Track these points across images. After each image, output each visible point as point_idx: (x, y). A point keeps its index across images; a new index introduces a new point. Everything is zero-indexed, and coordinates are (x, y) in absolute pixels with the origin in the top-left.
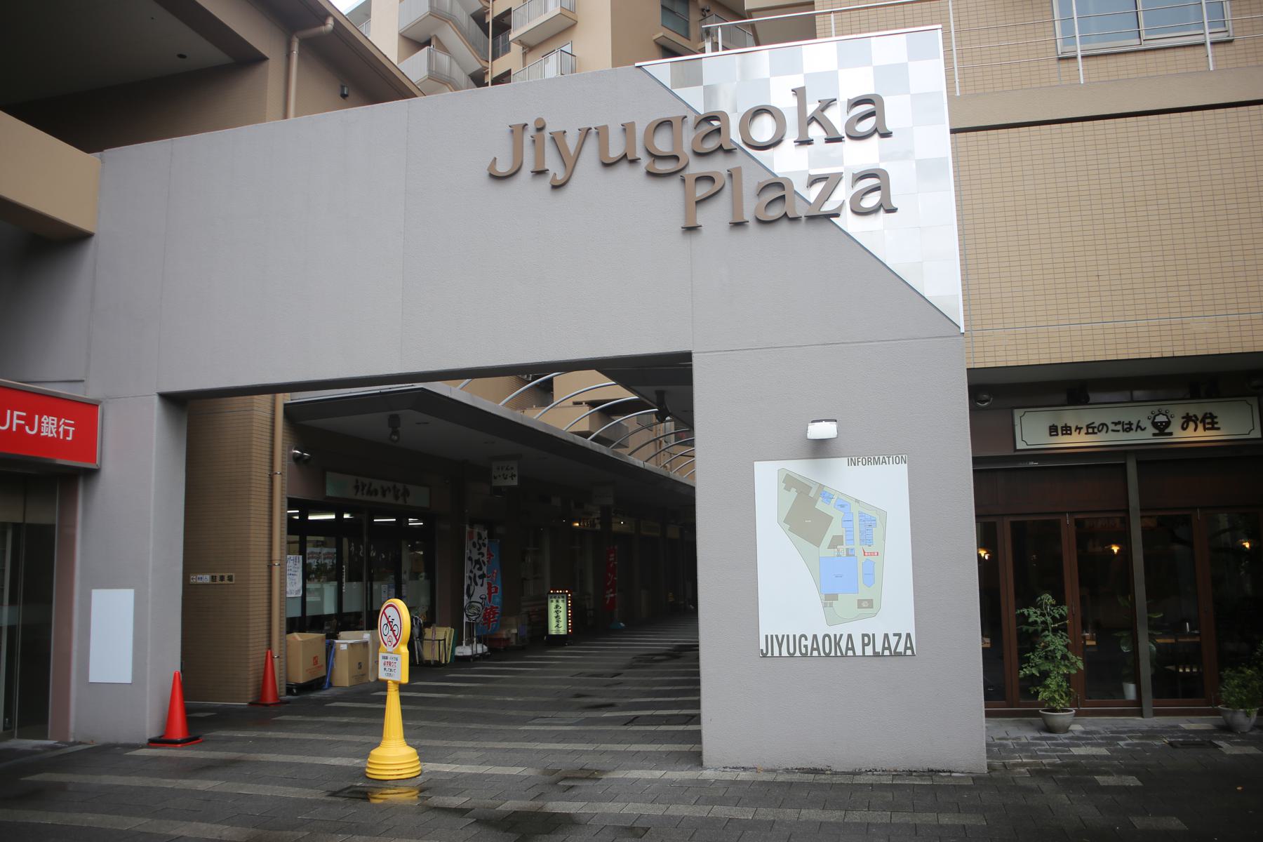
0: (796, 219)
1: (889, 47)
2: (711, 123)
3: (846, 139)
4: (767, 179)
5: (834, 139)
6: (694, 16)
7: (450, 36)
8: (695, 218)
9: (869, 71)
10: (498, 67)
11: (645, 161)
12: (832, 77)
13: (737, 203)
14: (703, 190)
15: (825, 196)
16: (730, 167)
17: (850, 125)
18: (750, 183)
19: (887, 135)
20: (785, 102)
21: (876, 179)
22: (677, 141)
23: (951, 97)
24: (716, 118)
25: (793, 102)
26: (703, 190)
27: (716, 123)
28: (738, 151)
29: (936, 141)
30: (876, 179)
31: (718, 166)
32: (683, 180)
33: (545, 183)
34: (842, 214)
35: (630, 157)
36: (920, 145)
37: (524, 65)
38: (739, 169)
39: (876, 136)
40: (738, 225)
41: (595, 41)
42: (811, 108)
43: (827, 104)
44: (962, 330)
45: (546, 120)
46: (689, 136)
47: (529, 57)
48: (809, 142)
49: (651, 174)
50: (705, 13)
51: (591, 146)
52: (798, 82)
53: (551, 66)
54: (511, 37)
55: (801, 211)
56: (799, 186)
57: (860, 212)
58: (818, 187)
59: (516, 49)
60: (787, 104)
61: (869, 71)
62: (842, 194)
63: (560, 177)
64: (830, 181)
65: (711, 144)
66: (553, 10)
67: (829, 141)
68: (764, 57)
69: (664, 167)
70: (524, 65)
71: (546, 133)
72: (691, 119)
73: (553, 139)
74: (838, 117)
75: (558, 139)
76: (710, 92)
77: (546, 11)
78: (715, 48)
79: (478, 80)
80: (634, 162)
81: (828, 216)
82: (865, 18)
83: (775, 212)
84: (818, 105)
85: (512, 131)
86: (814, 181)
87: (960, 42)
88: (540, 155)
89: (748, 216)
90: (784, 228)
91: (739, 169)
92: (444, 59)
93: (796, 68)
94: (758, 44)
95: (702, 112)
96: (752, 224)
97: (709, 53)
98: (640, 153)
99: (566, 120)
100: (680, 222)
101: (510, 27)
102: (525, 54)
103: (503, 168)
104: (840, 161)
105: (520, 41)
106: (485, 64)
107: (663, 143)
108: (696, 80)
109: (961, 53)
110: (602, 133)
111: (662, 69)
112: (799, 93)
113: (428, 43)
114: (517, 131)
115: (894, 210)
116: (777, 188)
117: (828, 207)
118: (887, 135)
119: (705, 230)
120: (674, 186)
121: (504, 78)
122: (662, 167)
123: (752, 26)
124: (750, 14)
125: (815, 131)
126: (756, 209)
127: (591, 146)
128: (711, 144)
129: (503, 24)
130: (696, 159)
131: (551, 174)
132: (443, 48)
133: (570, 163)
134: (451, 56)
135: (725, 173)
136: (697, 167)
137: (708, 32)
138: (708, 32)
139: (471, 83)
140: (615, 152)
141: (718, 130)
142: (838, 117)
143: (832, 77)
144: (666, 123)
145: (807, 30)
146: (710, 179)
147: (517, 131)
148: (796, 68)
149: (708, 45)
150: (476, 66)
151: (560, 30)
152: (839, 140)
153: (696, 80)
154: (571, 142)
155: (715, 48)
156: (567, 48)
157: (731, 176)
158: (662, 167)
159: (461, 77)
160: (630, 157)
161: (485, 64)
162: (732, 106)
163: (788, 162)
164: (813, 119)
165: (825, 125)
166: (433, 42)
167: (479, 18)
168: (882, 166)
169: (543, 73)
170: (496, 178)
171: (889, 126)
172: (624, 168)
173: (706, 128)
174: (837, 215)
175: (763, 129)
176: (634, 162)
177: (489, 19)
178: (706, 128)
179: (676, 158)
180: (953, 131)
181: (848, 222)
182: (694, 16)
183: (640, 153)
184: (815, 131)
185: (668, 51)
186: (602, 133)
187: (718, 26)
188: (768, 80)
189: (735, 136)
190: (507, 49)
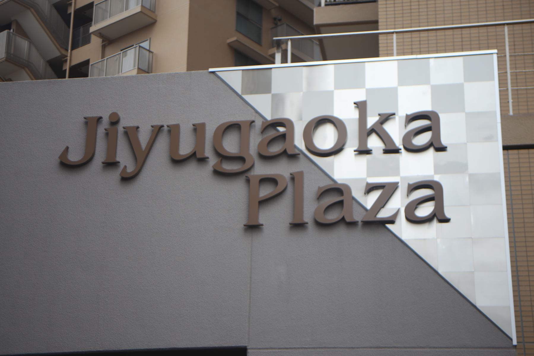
0: (352, 224)
1: (446, 68)
2: (277, 130)
3: (403, 151)
4: (325, 184)
5: (391, 150)
6: (266, 25)
7: (31, 23)
8: (257, 217)
9: (426, 89)
10: (78, 56)
11: (213, 161)
12: (392, 93)
13: (297, 205)
14: (266, 191)
15: (381, 203)
16: (292, 172)
17: (407, 138)
18: (311, 187)
19: (441, 149)
20: (348, 114)
21: (433, 190)
22: (244, 143)
23: (504, 116)
24: (282, 124)
25: (355, 114)
26: (266, 191)
27: (281, 129)
28: (301, 156)
29: (488, 158)
30: (433, 190)
31: (282, 169)
32: (248, 181)
33: (115, 176)
34: (397, 221)
35: (198, 156)
36: (475, 159)
37: (103, 57)
38: (301, 174)
39: (431, 151)
40: (298, 226)
41: (172, 43)
42: (372, 121)
43: (386, 118)
44: (515, 342)
45: (121, 115)
46: (255, 140)
47: (108, 50)
48: (368, 152)
49: (218, 173)
50: (276, 22)
51: (162, 145)
52: (361, 97)
53: (128, 62)
54: (92, 29)
55: (358, 217)
56: (357, 193)
57: (413, 220)
58: (375, 196)
59: (96, 42)
60: (348, 114)
61: (426, 89)
62: (398, 203)
63: (131, 169)
64: (388, 190)
65: (276, 149)
66: (134, 8)
67: (386, 152)
68: (328, 72)
69: (230, 168)
70: (103, 57)
71: (120, 128)
72: (259, 124)
73: (126, 133)
74: (395, 130)
75: (131, 134)
76: (278, 101)
77: (127, 8)
78: (284, 60)
79: (57, 68)
80: (203, 160)
81: (383, 223)
82: (424, 41)
83: (333, 216)
84: (377, 118)
85: (86, 123)
86: (371, 188)
87: (514, 66)
88: (112, 148)
89: (308, 217)
90: (341, 232)
91: (301, 174)
92: (24, 44)
93: (358, 82)
94: (325, 59)
95: (269, 118)
96: (311, 226)
97: (278, 64)
98: (208, 152)
99: (141, 117)
100: (240, 219)
101: (91, 20)
102: (104, 47)
103: (74, 157)
104: (396, 172)
105: (100, 33)
106: (64, 52)
107: (231, 145)
108: (264, 87)
109: (515, 76)
110: (174, 131)
111: (234, 75)
112: (361, 106)
113: (8, 27)
114: (91, 124)
115: (447, 220)
116: (336, 194)
117: (384, 214)
118: (441, 149)
119: (266, 229)
120: (237, 191)
121: (81, 70)
122: (228, 167)
123: (320, 40)
124: (317, 29)
125: (374, 143)
126: (316, 212)
127: (162, 145)
128: (276, 149)
129: (85, 16)
130: (264, 162)
131: (122, 167)
132: (23, 33)
133: (141, 157)
134: (31, 42)
135: (287, 176)
136: (261, 170)
137: (278, 44)
138: (278, 44)
139: (49, 70)
140: (185, 148)
141: (283, 137)
142: (395, 130)
143: (392, 93)
144: (234, 126)
145: (370, 48)
146: (272, 180)
147: (91, 124)
148: (358, 82)
149: (278, 57)
150: (54, 52)
151: (139, 28)
152: (396, 151)
153: (264, 87)
154: (144, 138)
155: (284, 60)
156: (145, 45)
157: (293, 179)
158: (228, 167)
159: (40, 64)
160: (198, 156)
161: (64, 52)
162: (297, 112)
163: (348, 169)
164: (372, 131)
165: (384, 137)
166: (14, 27)
167: (61, 8)
168: (437, 178)
169: (120, 70)
170: (67, 166)
171: (444, 141)
172: (192, 168)
173: (271, 134)
174: (392, 222)
175: (326, 138)
176: (203, 160)
177: (72, 10)
178: (271, 134)
179: (241, 159)
180: (506, 148)
181: (403, 230)
182: (266, 25)
183: (208, 152)
184: (374, 143)
185: (241, 57)
186: (174, 131)
187: (289, 40)
188: (331, 93)
189: (299, 142)
190: (87, 40)
